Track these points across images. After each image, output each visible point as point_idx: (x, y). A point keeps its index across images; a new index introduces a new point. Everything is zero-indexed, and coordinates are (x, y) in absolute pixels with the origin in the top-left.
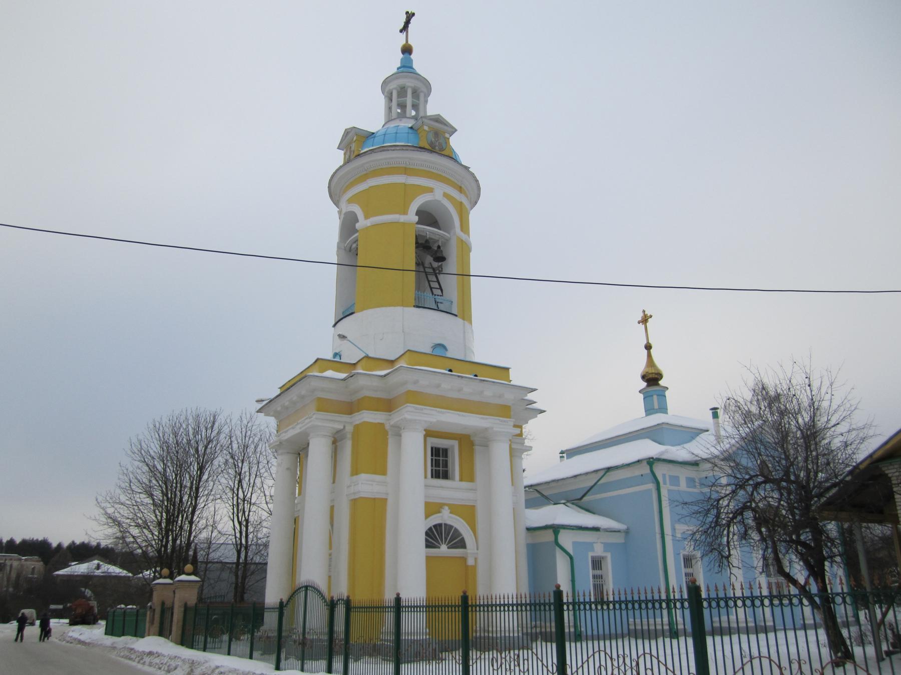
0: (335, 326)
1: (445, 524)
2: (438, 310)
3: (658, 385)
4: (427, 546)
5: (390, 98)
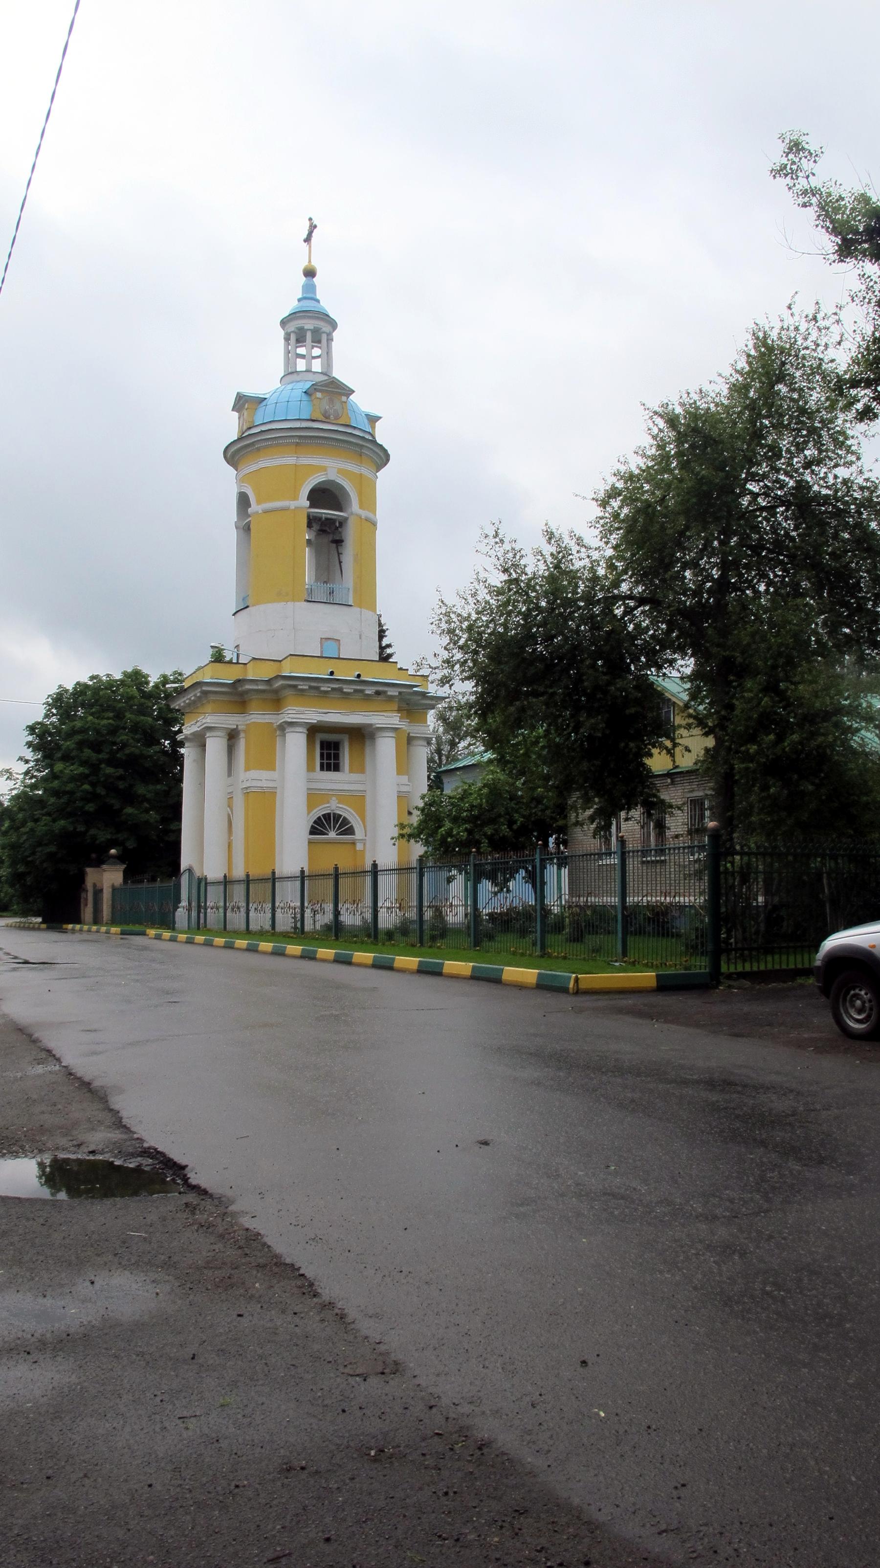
0: (234, 615)
1: (334, 814)
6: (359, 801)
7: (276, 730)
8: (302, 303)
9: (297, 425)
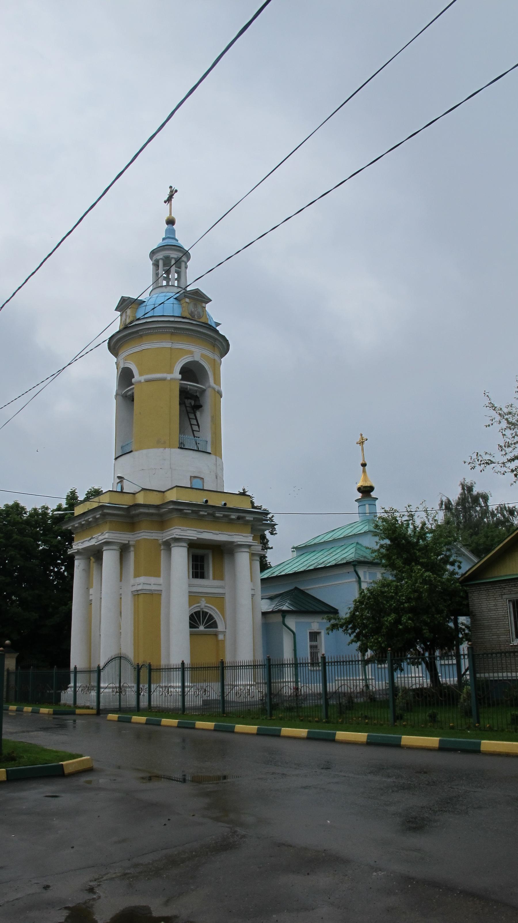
1: (203, 612)
2: (198, 451)
3: (370, 496)
4: (191, 627)
5: (156, 265)
6: (219, 600)
7: (160, 545)
8: (165, 241)
9: (172, 319)
